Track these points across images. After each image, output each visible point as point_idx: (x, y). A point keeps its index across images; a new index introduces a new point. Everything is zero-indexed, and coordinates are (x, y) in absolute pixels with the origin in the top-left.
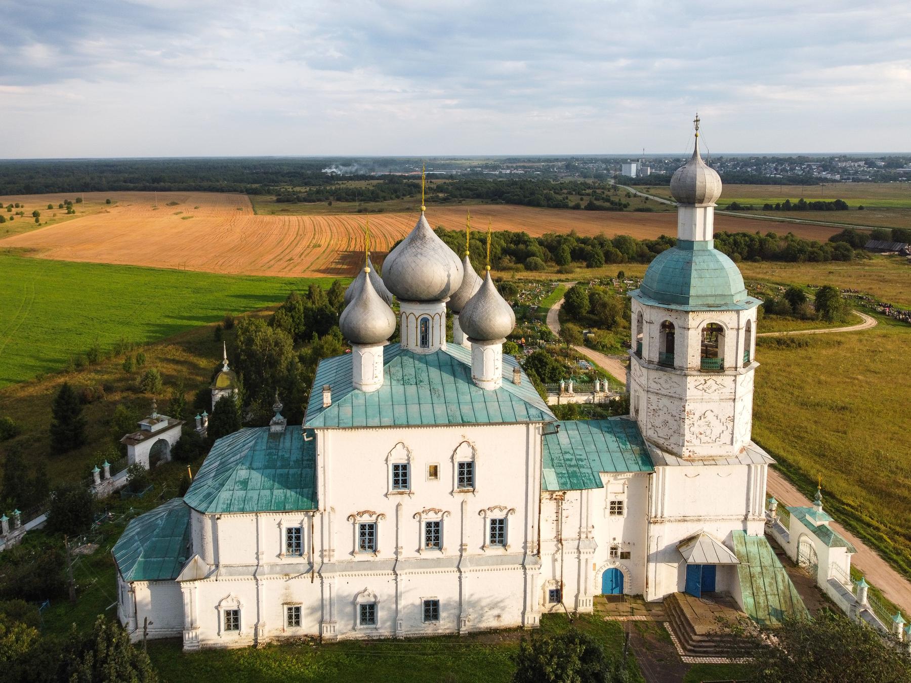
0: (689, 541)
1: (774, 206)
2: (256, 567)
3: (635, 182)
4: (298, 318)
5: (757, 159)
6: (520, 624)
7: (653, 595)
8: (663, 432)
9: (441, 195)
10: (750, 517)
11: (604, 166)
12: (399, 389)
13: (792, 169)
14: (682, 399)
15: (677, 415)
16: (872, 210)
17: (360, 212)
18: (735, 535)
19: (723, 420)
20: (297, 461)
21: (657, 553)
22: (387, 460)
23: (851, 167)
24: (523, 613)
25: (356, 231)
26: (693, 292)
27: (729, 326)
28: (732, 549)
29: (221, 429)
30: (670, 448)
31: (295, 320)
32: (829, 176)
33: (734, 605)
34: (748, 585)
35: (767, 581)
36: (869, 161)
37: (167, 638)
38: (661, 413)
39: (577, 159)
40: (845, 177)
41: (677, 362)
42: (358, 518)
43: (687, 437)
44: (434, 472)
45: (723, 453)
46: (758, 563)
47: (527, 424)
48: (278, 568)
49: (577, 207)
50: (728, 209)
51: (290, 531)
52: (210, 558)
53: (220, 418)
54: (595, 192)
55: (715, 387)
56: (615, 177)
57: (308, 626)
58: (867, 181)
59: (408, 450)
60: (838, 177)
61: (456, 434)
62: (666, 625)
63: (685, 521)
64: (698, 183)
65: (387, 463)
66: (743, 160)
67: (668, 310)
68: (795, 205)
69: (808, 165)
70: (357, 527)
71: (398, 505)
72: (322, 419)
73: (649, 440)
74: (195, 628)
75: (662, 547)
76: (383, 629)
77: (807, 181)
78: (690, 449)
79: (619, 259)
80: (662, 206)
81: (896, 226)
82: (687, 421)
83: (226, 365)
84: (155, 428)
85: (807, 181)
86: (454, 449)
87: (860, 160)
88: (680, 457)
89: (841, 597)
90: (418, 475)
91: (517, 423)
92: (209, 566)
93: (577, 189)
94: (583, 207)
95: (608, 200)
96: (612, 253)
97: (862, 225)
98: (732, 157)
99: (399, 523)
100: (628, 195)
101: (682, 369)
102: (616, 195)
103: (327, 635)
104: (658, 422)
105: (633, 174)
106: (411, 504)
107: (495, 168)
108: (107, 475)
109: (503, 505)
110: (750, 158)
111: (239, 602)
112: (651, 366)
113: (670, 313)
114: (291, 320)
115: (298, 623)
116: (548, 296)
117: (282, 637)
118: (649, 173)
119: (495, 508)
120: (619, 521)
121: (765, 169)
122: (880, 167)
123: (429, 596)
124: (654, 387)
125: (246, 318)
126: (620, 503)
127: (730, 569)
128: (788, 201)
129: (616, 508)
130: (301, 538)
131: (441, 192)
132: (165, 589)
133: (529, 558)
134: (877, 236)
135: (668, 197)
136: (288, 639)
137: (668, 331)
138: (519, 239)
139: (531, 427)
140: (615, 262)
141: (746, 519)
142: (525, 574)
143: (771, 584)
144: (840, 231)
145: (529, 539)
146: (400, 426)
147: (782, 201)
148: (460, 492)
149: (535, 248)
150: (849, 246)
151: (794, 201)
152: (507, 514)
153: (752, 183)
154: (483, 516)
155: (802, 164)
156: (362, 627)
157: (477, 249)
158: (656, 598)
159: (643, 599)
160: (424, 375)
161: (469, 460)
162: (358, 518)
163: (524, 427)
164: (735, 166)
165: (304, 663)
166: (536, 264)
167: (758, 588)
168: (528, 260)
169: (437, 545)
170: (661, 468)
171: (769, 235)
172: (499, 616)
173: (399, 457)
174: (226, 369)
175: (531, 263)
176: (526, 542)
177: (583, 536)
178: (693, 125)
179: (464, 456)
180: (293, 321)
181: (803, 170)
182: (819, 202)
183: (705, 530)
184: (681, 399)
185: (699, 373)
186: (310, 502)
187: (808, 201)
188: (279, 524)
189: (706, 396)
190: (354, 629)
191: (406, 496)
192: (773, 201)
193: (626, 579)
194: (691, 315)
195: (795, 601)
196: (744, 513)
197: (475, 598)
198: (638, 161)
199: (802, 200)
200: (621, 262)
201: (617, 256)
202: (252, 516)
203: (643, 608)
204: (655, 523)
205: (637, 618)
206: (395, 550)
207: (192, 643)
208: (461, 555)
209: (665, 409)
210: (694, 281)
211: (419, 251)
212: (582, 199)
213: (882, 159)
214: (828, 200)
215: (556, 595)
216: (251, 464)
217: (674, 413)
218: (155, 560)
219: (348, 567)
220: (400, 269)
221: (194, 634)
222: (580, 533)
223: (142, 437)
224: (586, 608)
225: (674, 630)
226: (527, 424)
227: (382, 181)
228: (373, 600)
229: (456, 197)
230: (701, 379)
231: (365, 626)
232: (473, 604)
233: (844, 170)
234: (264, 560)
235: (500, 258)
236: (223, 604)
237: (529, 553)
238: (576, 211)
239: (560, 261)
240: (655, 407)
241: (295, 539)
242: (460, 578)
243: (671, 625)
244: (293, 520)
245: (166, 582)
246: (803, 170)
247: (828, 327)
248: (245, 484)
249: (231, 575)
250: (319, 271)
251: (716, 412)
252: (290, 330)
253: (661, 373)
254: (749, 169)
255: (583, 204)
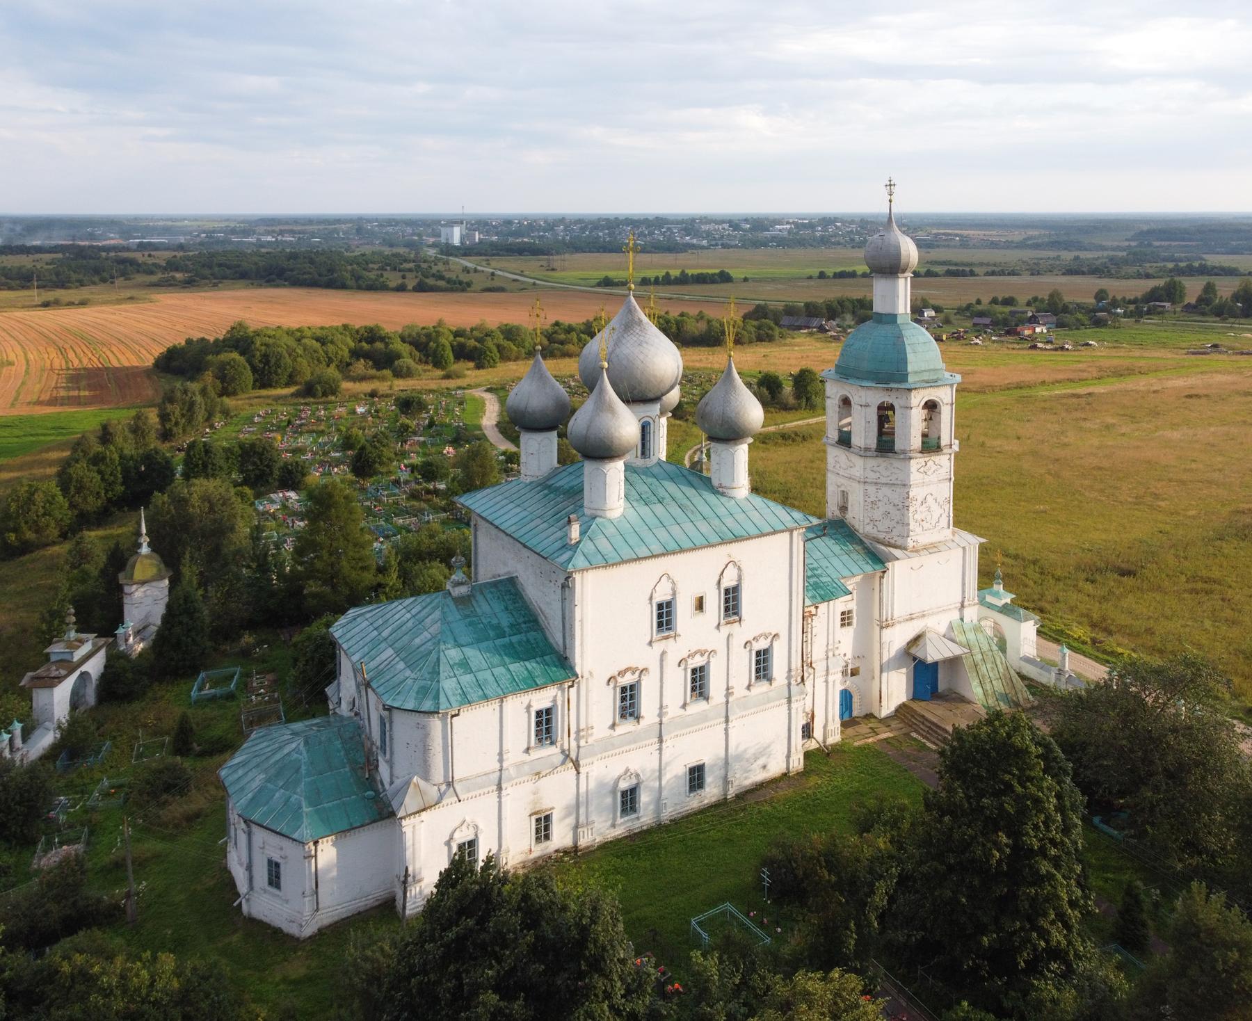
0: (917, 639)
1: (652, 280)
2: (498, 773)
3: (466, 251)
4: (111, 475)
5: (607, 220)
6: (785, 771)
7: (887, 709)
8: (883, 526)
9: (179, 276)
10: (966, 603)
11: (409, 230)
12: (644, 510)
13: (651, 234)
14: (905, 485)
15: (900, 504)
16: (757, 281)
17: (46, 305)
18: (955, 625)
19: (941, 503)
20: (512, 626)
21: (889, 661)
22: (651, 598)
23: (715, 230)
24: (788, 756)
25: (63, 337)
26: (910, 369)
27: (945, 401)
28: (953, 641)
29: (184, 638)
30: (892, 541)
31: (106, 477)
32: (695, 241)
33: (963, 700)
34: (975, 674)
35: (989, 666)
36: (734, 224)
37: (359, 913)
38: (880, 504)
39: (369, 220)
40: (713, 243)
41: (898, 447)
42: (619, 679)
43: (911, 527)
44: (700, 604)
45: (942, 538)
46: (978, 650)
47: (791, 531)
48: (526, 768)
49: (401, 289)
50: (599, 285)
51: (539, 714)
52: (438, 774)
53: (181, 623)
54: (419, 266)
55: (934, 467)
56: (434, 245)
57: (561, 837)
58: (736, 246)
59: (673, 583)
60: (705, 242)
61: (719, 555)
62: (914, 735)
63: (912, 619)
64: (903, 252)
65: (651, 603)
66: (591, 222)
67: (887, 389)
68: (676, 278)
69: (669, 229)
70: (618, 690)
71: (663, 653)
72: (582, 558)
73: (867, 536)
74: (420, 881)
75: (893, 653)
76: (645, 816)
77: (671, 248)
78: (914, 538)
79: (514, 355)
80: (516, 284)
81: (809, 300)
82: (911, 508)
83: (145, 545)
84: (78, 654)
85: (671, 248)
86: (720, 572)
87: (723, 222)
88: (906, 549)
89: (1039, 670)
90: (683, 610)
91: (775, 532)
92: (436, 788)
93: (392, 263)
94: (410, 287)
95: (441, 278)
96: (504, 348)
97: (776, 298)
98: (577, 218)
99: (665, 675)
100: (466, 270)
101: (904, 452)
102: (449, 270)
103: (583, 842)
104: (877, 514)
105: (456, 241)
106: (676, 649)
107: (246, 232)
108: (18, 742)
109: (767, 631)
110: (600, 219)
111: (476, 827)
112: (868, 454)
113: (889, 393)
114: (99, 477)
115: (547, 837)
116: (464, 410)
117: (528, 861)
118: (477, 240)
119: (760, 636)
120: (849, 632)
121: (620, 234)
122: (744, 231)
123: (693, 762)
124: (872, 476)
125: (25, 482)
126: (850, 612)
127: (953, 663)
128: (668, 274)
129: (846, 619)
130: (554, 721)
131: (177, 270)
132: (369, 838)
133: (794, 689)
134: (790, 311)
135: (518, 272)
136: (535, 861)
137: (885, 414)
138: (372, 335)
139: (795, 533)
140: (509, 360)
141: (963, 606)
142: (789, 709)
143: (992, 668)
144: (751, 308)
145: (793, 667)
146: (674, 553)
147: (661, 273)
148: (728, 623)
149: (398, 346)
150: (772, 324)
151: (675, 273)
152: (772, 642)
153: (611, 251)
154: (748, 649)
155: (660, 227)
156: (622, 820)
157: (315, 351)
158: (889, 712)
159: (875, 717)
160: (661, 492)
161: (668, 598)
162: (619, 679)
163: (787, 535)
164: (583, 230)
165: (575, 882)
166: (408, 368)
167: (983, 676)
168: (396, 363)
169: (701, 694)
170: (890, 564)
171: (682, 315)
172: (764, 767)
173: (662, 595)
174: (145, 550)
175: (401, 367)
176: (790, 670)
177: (830, 654)
178: (885, 191)
179: (729, 582)
180: (103, 479)
181: (663, 234)
182: (702, 274)
183: (929, 625)
184: (904, 485)
185: (921, 455)
186: (562, 671)
187: (690, 272)
188: (528, 707)
189: (927, 479)
190: (613, 826)
191: (671, 640)
192: (651, 274)
193: (855, 700)
194: (913, 393)
195: (1014, 681)
196: (960, 600)
197: (741, 748)
198: (462, 223)
199: (683, 272)
200: (516, 359)
201: (511, 349)
202: (495, 705)
203: (880, 725)
204: (887, 626)
205: (883, 736)
206: (658, 712)
207: (414, 903)
208: (727, 702)
209: (886, 500)
210: (910, 357)
211: (642, 338)
212: (404, 277)
213: (746, 220)
214: (711, 271)
215: (807, 731)
216: (455, 641)
217: (896, 502)
218: (330, 804)
219: (607, 747)
220: (625, 362)
221: (418, 889)
222: (827, 652)
223: (63, 672)
224: (835, 738)
225: (925, 737)
226: (791, 531)
227: (60, 256)
228: (634, 781)
229: (205, 278)
230: (922, 461)
231: (626, 818)
232: (739, 758)
233: (708, 234)
234: (510, 760)
235: (348, 364)
236: (456, 836)
237: (793, 682)
238: (400, 294)
239: (438, 363)
240: (873, 499)
241: (545, 724)
242: (726, 730)
243: (919, 733)
244: (541, 699)
245: (366, 828)
246: (663, 234)
247: (814, 417)
248: (465, 665)
249: (469, 791)
250: (39, 403)
251: (935, 496)
252: (98, 493)
253: (880, 460)
254: (601, 234)
255: (411, 284)
